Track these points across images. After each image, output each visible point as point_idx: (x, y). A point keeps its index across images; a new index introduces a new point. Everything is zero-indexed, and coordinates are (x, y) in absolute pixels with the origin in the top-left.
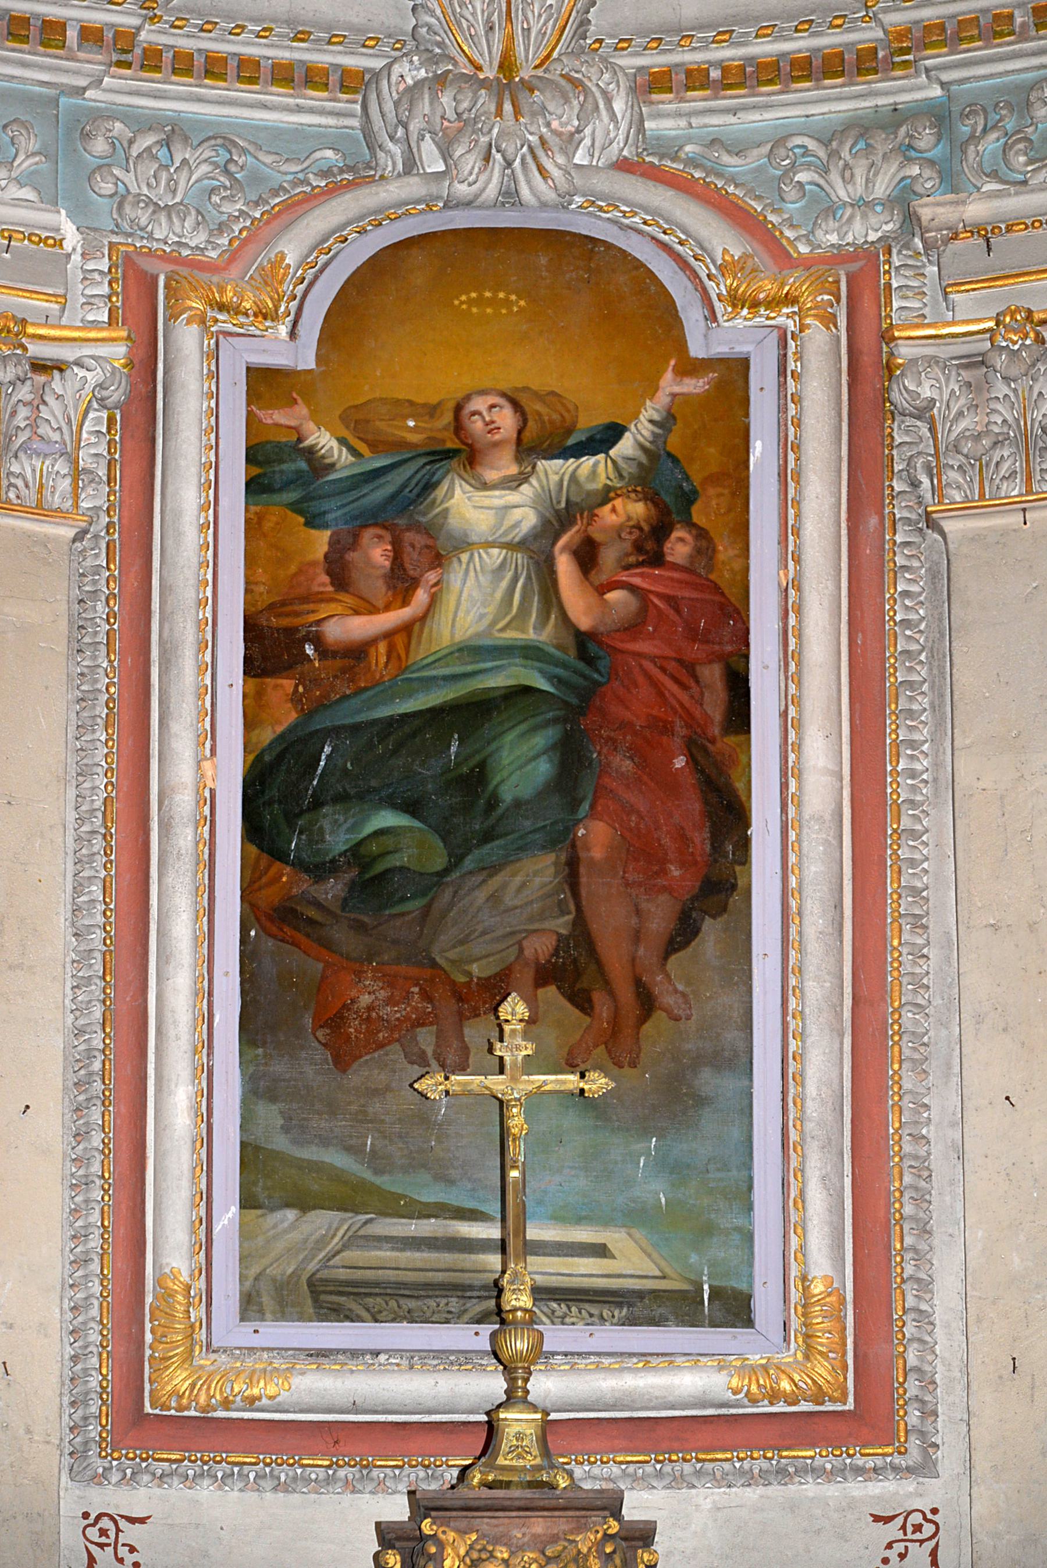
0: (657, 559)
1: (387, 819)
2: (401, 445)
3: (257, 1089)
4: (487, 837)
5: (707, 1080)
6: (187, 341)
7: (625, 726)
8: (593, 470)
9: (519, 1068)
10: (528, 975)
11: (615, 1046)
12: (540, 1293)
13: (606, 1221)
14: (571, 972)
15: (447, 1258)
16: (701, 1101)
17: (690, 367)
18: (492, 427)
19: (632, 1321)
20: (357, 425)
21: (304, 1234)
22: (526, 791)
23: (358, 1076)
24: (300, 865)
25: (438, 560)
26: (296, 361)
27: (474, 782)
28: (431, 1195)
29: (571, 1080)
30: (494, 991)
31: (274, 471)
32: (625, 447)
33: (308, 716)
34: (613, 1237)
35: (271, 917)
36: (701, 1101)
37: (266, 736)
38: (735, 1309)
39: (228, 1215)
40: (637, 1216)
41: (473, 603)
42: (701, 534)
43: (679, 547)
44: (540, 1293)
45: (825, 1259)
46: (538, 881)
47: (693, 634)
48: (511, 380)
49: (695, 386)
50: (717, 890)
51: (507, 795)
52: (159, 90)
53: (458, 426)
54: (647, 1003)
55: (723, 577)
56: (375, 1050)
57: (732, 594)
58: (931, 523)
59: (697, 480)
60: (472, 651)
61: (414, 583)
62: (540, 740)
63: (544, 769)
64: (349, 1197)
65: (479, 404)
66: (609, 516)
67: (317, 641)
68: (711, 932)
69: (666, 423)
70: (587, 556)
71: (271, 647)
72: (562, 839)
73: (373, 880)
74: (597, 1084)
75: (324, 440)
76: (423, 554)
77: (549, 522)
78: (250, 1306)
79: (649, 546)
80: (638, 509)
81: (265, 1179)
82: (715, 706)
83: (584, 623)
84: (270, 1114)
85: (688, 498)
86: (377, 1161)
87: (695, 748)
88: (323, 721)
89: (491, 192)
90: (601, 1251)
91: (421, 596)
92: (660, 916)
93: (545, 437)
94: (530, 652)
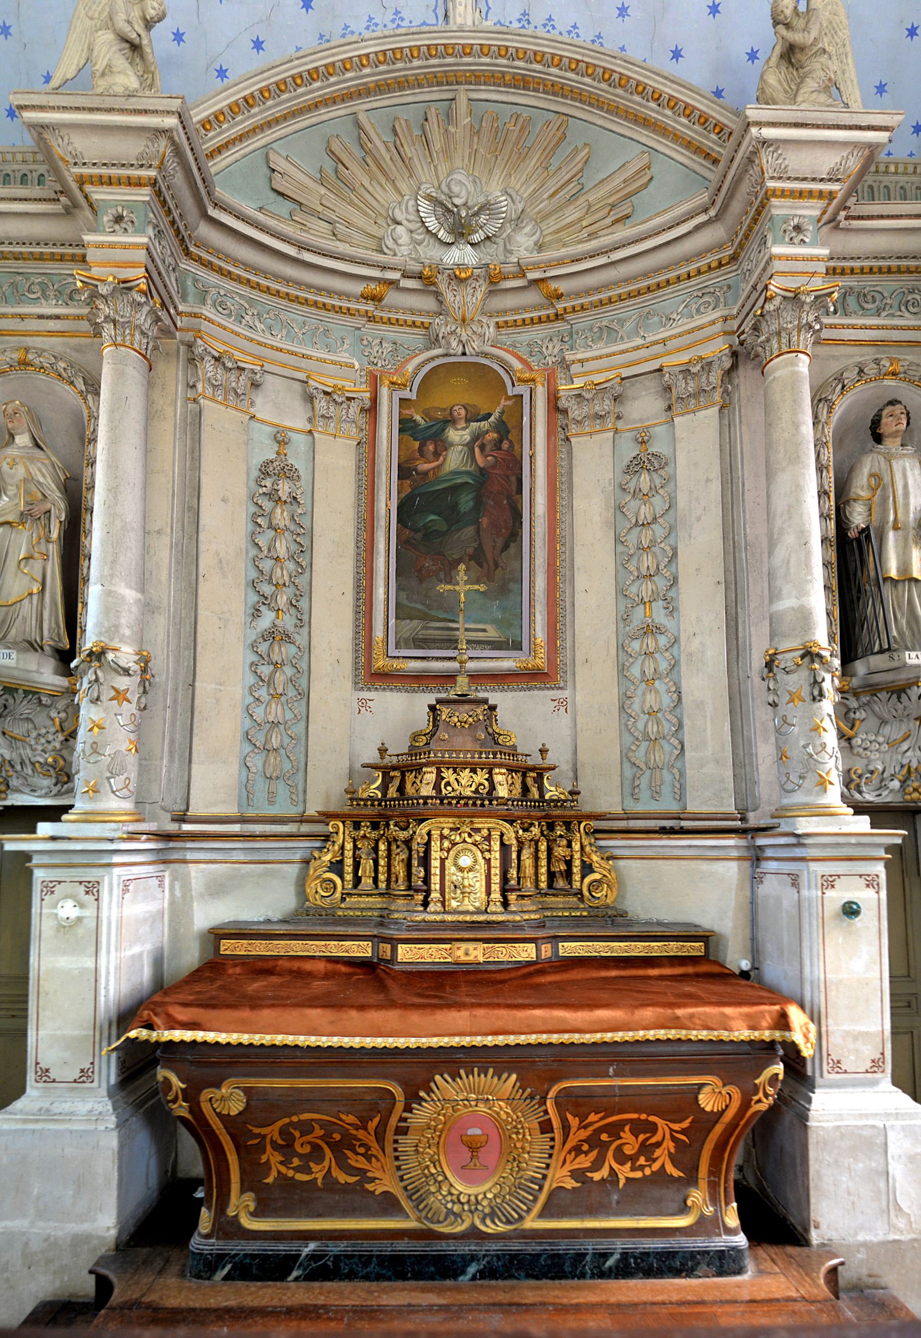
0: (500, 449)
1: (433, 517)
3: (399, 588)
4: (457, 522)
5: (512, 586)
6: (384, 392)
7: (491, 493)
8: (484, 425)
9: (463, 585)
10: (467, 558)
11: (489, 577)
12: (468, 642)
13: (486, 623)
14: (477, 557)
15: (446, 632)
16: (510, 591)
17: (508, 398)
18: (459, 414)
19: (492, 649)
20: (426, 414)
21: (412, 626)
22: (467, 510)
23: (424, 585)
24: (411, 529)
25: (446, 449)
27: (454, 507)
28: (443, 615)
29: (477, 587)
30: (459, 561)
31: (406, 426)
32: (492, 419)
36: (510, 591)
37: (403, 495)
38: (518, 646)
39: (392, 622)
40: (494, 622)
41: (454, 460)
42: (511, 442)
43: (505, 445)
44: (468, 642)
45: (541, 635)
47: (508, 467)
48: (464, 402)
49: (509, 403)
50: (514, 536)
51: (462, 510)
52: (625, 968)
53: (451, 414)
54: (497, 565)
55: (516, 453)
56: (324, 1306)
57: (518, 458)
58: (568, 439)
59: (510, 427)
61: (440, 455)
62: (471, 496)
63: (471, 504)
64: (424, 617)
65: (456, 408)
66: (489, 437)
67: (416, 470)
68: (513, 548)
70: (482, 448)
71: (404, 472)
73: (429, 535)
74: (482, 588)
75: (418, 418)
76: (443, 446)
77: (162, 948)
78: (397, 646)
79: (498, 445)
80: (495, 435)
81: (402, 613)
82: (514, 488)
83: (482, 465)
84: (403, 595)
85: (508, 432)
86: (429, 607)
87: (509, 497)
88: (416, 492)
89: (460, 352)
90: (484, 630)
91: (441, 458)
92: (500, 543)
94: (467, 473)
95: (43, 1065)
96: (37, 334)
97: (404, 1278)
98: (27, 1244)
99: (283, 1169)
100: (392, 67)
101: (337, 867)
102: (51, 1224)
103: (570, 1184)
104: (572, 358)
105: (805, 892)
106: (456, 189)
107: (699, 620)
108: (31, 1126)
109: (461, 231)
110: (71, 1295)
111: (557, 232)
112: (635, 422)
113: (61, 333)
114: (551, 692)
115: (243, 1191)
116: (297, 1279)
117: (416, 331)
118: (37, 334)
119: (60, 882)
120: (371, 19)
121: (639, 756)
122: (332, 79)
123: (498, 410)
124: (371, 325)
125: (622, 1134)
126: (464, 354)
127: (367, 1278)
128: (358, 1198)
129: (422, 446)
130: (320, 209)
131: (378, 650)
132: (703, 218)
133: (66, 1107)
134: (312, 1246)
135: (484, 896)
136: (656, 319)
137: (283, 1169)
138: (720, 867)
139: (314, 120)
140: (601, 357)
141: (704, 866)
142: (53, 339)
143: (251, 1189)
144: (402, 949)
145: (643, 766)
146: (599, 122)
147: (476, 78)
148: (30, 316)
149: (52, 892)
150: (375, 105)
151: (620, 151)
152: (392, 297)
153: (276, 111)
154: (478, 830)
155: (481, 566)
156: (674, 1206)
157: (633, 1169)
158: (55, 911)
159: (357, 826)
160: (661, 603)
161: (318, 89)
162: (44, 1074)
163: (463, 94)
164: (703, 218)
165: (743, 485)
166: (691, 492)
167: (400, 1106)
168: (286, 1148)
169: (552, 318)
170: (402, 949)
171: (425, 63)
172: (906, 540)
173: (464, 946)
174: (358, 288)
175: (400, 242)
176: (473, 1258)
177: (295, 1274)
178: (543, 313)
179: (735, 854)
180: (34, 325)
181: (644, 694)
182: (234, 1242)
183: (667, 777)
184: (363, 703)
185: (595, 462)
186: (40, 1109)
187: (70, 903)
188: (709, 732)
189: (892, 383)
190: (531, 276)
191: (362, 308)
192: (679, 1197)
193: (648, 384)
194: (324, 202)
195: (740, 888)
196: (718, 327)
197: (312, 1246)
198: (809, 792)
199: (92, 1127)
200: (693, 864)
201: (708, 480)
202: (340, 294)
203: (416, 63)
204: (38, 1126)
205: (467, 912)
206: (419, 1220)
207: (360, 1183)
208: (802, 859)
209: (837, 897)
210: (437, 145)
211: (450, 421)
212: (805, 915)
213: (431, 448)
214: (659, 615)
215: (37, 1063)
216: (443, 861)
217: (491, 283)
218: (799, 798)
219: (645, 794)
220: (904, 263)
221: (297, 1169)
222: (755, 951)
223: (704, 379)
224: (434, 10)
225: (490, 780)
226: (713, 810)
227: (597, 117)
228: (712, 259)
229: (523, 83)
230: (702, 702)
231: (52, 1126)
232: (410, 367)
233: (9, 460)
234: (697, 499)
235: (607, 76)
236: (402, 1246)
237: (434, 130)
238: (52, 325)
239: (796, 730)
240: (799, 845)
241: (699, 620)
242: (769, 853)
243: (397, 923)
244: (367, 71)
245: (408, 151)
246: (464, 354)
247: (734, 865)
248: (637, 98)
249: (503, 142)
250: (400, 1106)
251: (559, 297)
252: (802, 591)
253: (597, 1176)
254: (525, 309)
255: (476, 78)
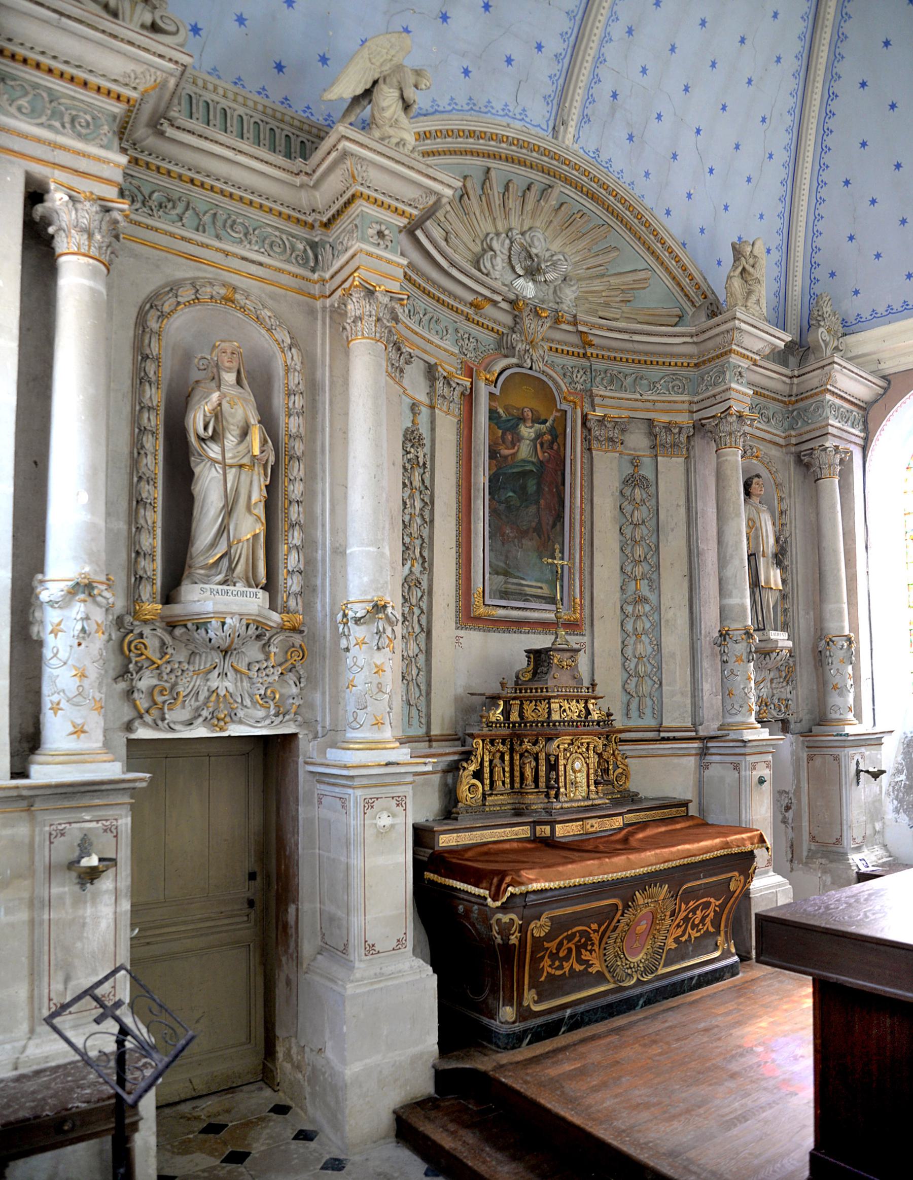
0: (552, 448)
2: (513, 415)
13: (542, 582)
14: (538, 530)
17: (558, 411)
20: (506, 409)
25: (519, 441)
26: (113, 1034)
27: (524, 488)
31: (493, 415)
32: (548, 424)
33: (498, 470)
34: (543, 585)
35: (493, 512)
37: (492, 472)
41: (524, 451)
46: (763, 1024)
53: (523, 413)
60: (524, 461)
62: (534, 482)
68: (558, 527)
69: (554, 421)
70: (542, 445)
71: (493, 454)
72: (537, 502)
75: (501, 411)
82: (560, 480)
87: (557, 487)
88: (501, 471)
90: (541, 588)
93: (537, 420)
94: (533, 463)
95: (370, 942)
96: (237, 272)
97: (613, 1016)
98: (381, 1072)
99: (550, 970)
100: (519, 150)
101: (478, 775)
102: (397, 1052)
103: (674, 946)
104: (597, 392)
105: (743, 773)
106: (536, 243)
107: (672, 598)
108: (376, 986)
109: (532, 272)
110: (412, 1099)
111: (586, 292)
112: (631, 450)
113: (261, 279)
114: (576, 637)
115: (529, 990)
116: (563, 1033)
117: (492, 334)
118: (237, 272)
119: (377, 799)
120: (506, 105)
121: (631, 687)
122: (481, 141)
123: (551, 418)
124: (466, 322)
125: (533, 991)
126: (531, 368)
127: (596, 1021)
128: (583, 978)
129: (504, 434)
130: (443, 219)
131: (477, 599)
132: (688, 339)
133: (392, 968)
134: (569, 1012)
135: (585, 788)
136: (645, 381)
137: (550, 970)
138: (684, 760)
139: (461, 161)
140: (614, 398)
141: (676, 760)
142: (254, 282)
143: (533, 987)
144: (558, 827)
145: (634, 694)
146: (628, 239)
147: (567, 180)
148: (235, 255)
149: (372, 807)
150: (500, 167)
151: (634, 258)
152: (488, 309)
153: (440, 147)
154: (582, 744)
155: (540, 538)
156: (712, 948)
157: (697, 932)
158: (375, 822)
159: (492, 742)
160: (646, 581)
161: (470, 144)
162: (371, 949)
163: (560, 188)
164: (688, 339)
165: (697, 513)
166: (668, 510)
167: (620, 913)
168: (554, 956)
169: (581, 355)
170: (558, 827)
171: (539, 157)
172: (768, 564)
173: (591, 822)
174: (470, 297)
175: (496, 268)
176: (640, 996)
177: (563, 1030)
178: (576, 350)
179: (694, 752)
180: (236, 263)
181: (635, 644)
182: (529, 1022)
183: (649, 702)
184: (458, 638)
185: (608, 471)
186: (375, 974)
187: (385, 815)
188: (678, 673)
189: (756, 462)
190: (581, 328)
191: (466, 310)
192: (713, 943)
193: (639, 425)
194: (448, 216)
195: (695, 774)
196: (686, 406)
197: (569, 1012)
198: (744, 715)
199: (418, 977)
200: (668, 759)
201: (678, 505)
202: (456, 297)
203: (534, 154)
204: (382, 985)
205: (579, 800)
206: (615, 983)
207: (586, 969)
208: (744, 754)
209: (757, 774)
210: (529, 207)
211: (522, 419)
212: (743, 786)
213: (510, 437)
214: (645, 590)
215: (366, 941)
216: (565, 766)
217: (556, 322)
218: (738, 718)
219: (634, 713)
220: (763, 391)
221: (557, 969)
222: (701, 809)
223: (677, 436)
224: (547, 121)
225: (586, 708)
226: (679, 725)
227: (627, 236)
228: (686, 361)
229: (593, 197)
230: (674, 654)
231: (390, 983)
232: (497, 369)
233: (228, 399)
234: (672, 516)
235: (639, 216)
236: (611, 999)
237: (532, 196)
238: (253, 269)
239: (739, 678)
240: (745, 746)
241: (672, 598)
242: (712, 751)
243: (537, 812)
244: (504, 145)
245: (511, 204)
246: (531, 368)
247: (692, 759)
248: (652, 237)
249: (569, 222)
250: (620, 913)
251: (591, 345)
252: (743, 597)
253: (683, 939)
254: (566, 344)
255: (567, 180)
